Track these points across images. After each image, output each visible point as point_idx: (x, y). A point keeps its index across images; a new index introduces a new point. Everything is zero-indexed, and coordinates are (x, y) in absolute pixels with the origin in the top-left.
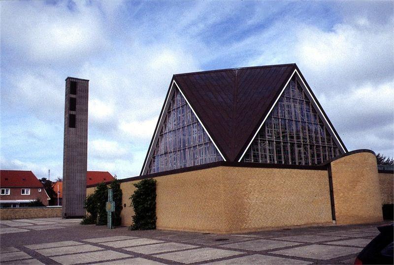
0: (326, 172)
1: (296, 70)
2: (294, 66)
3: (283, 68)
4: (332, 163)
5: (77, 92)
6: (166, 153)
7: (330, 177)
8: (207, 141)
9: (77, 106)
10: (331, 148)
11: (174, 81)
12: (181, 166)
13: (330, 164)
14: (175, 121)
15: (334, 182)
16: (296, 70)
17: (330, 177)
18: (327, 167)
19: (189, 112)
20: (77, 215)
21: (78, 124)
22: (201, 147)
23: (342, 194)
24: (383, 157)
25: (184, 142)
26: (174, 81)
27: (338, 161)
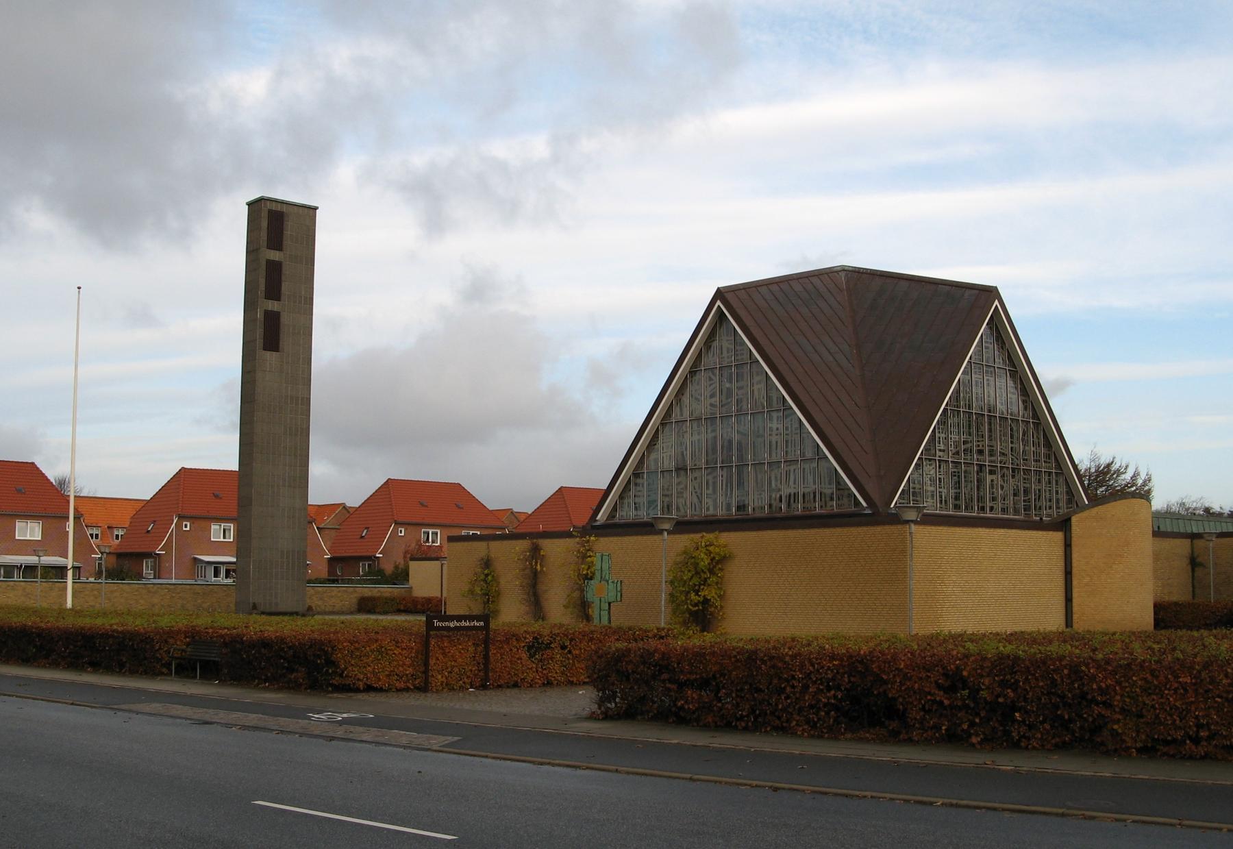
0: (1058, 536)
1: (996, 302)
2: (989, 294)
3: (968, 293)
4: (1074, 519)
5: (280, 243)
6: (681, 469)
7: (1068, 546)
8: (809, 455)
9: (285, 287)
10: (1050, 473)
11: (719, 303)
12: (729, 507)
13: (1070, 519)
14: (712, 396)
15: (1075, 556)
16: (996, 302)
17: (1068, 546)
18: (1063, 525)
19: (759, 382)
20: (282, 608)
21: (286, 341)
22: (792, 468)
23: (1087, 580)
24: (1124, 465)
25: (740, 450)
26: (719, 303)
27: (1085, 514)
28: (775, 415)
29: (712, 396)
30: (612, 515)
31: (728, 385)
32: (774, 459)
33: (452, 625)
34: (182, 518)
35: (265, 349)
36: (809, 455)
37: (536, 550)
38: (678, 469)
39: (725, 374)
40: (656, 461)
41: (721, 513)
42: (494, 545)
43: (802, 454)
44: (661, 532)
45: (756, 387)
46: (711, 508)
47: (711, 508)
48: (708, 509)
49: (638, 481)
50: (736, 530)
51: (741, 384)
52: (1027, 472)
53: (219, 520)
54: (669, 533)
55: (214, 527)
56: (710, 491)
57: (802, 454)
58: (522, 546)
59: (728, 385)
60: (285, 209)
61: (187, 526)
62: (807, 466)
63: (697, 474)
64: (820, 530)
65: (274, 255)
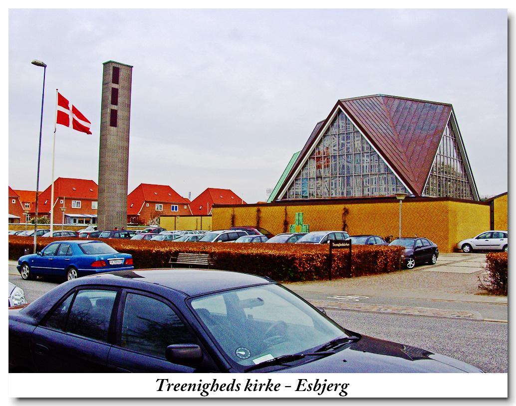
0: (488, 207)
7: (492, 211)
8: (382, 172)
11: (339, 106)
12: (343, 193)
13: (493, 201)
17: (492, 211)
21: (120, 122)
26: (339, 106)
28: (365, 155)
29: (334, 146)
30: (285, 197)
31: (342, 142)
32: (365, 173)
33: (204, 255)
34: (147, 202)
35: (111, 126)
36: (382, 172)
37: (259, 211)
38: (317, 177)
39: (341, 136)
40: (307, 174)
41: (339, 196)
42: (236, 209)
43: (379, 171)
44: (398, 201)
45: (356, 143)
46: (334, 194)
47: (334, 194)
48: (332, 194)
49: (297, 182)
50: (317, 204)
51: (348, 141)
52: (459, 181)
53: (158, 203)
54: (403, 201)
55: (73, 202)
56: (333, 187)
57: (379, 171)
58: (255, 209)
59: (342, 142)
60: (119, 66)
61: (148, 205)
62: (381, 176)
63: (327, 179)
64: (217, 209)
65: (115, 86)
